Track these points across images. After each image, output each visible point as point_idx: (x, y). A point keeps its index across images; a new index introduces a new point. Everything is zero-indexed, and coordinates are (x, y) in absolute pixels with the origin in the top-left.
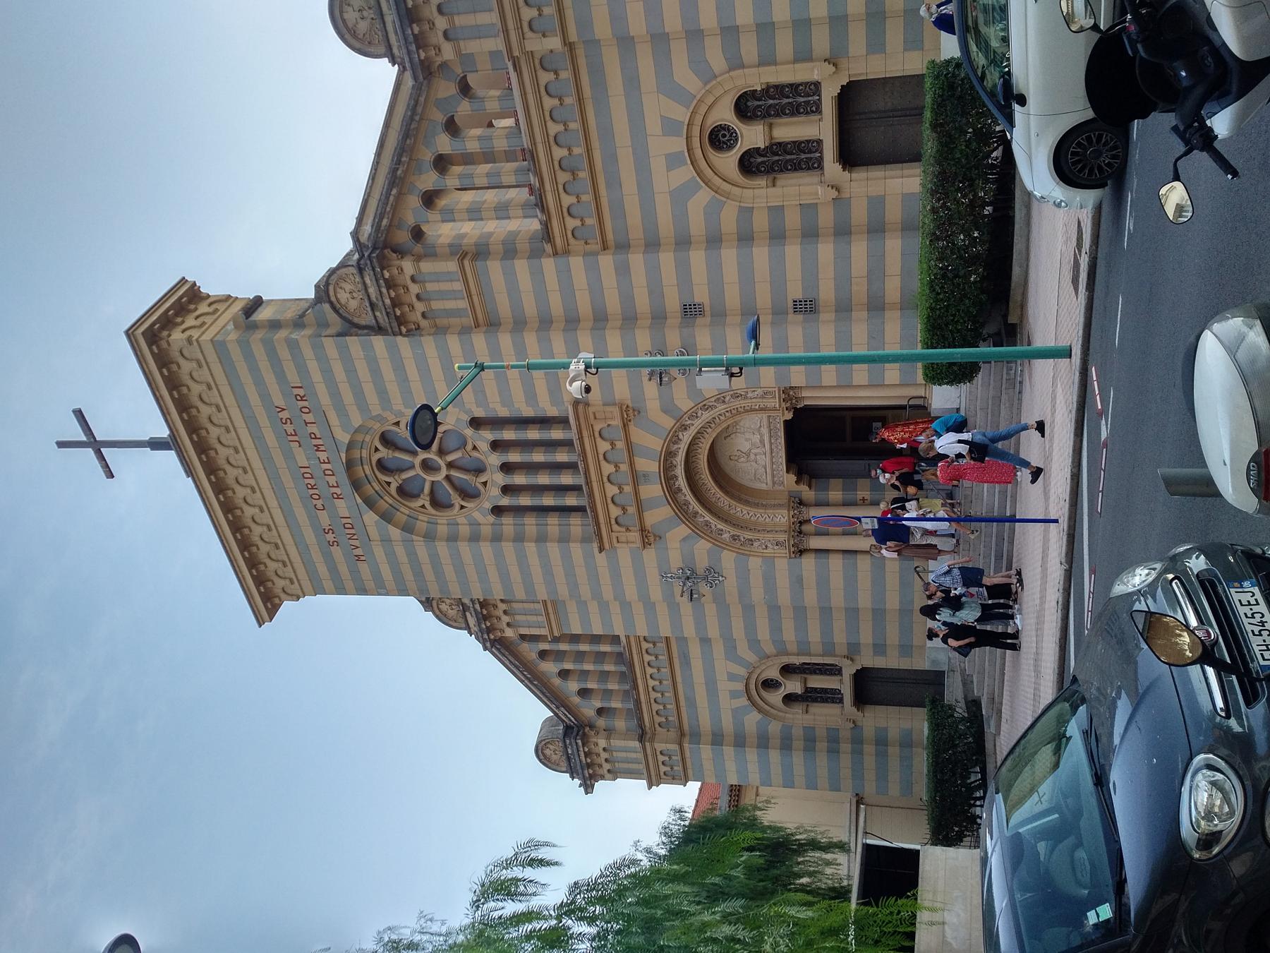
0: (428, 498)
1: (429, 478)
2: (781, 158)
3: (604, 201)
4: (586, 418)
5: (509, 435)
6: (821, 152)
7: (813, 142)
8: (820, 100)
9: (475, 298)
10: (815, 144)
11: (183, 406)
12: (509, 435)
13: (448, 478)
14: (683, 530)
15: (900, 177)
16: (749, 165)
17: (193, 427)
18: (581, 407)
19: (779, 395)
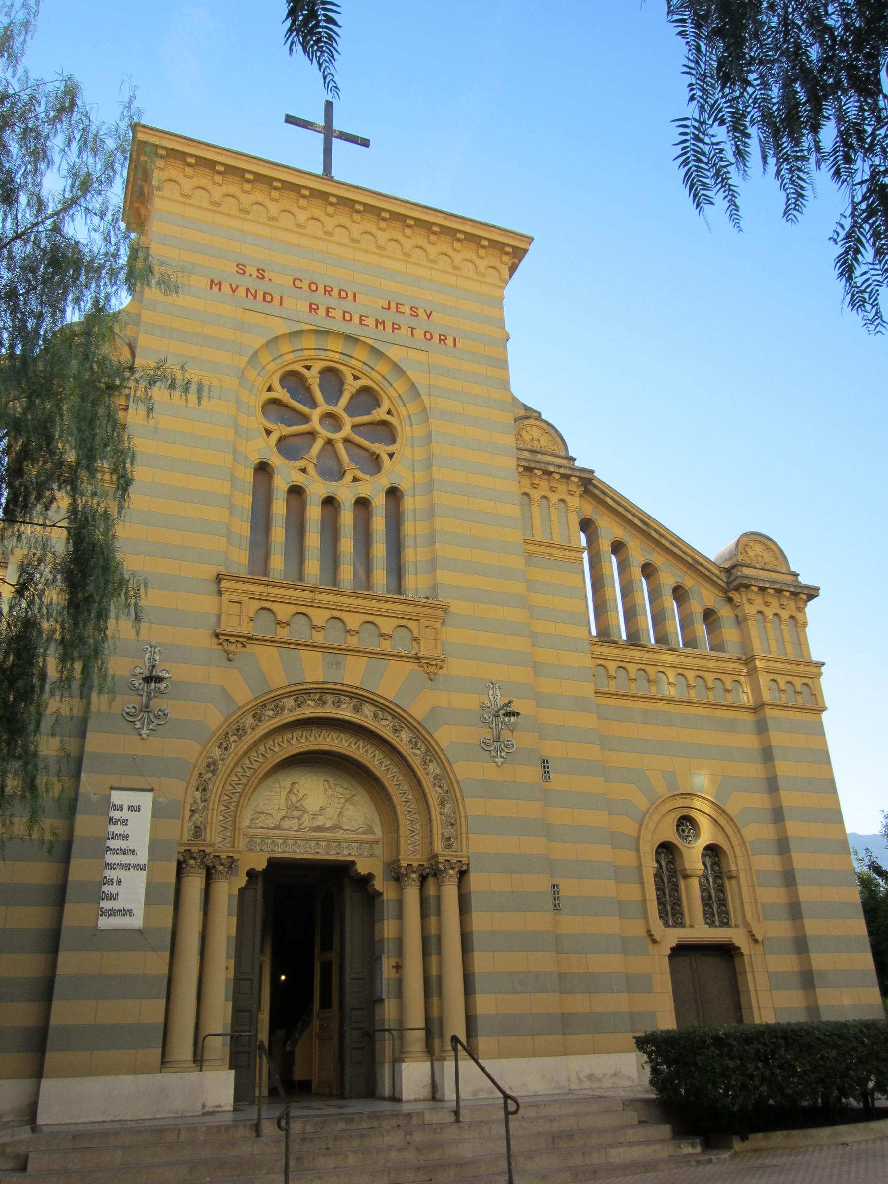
0: (346, 386)
1: (324, 407)
2: (666, 885)
3: (629, 704)
4: (429, 616)
5: (379, 523)
6: (674, 926)
7: (681, 919)
8: (716, 926)
9: (546, 550)
10: (680, 920)
11: (347, 203)
12: (379, 523)
13: (355, 427)
14: (243, 695)
15: (751, 958)
16: (666, 849)
17: (323, 196)
18: (441, 613)
19: (457, 856)
